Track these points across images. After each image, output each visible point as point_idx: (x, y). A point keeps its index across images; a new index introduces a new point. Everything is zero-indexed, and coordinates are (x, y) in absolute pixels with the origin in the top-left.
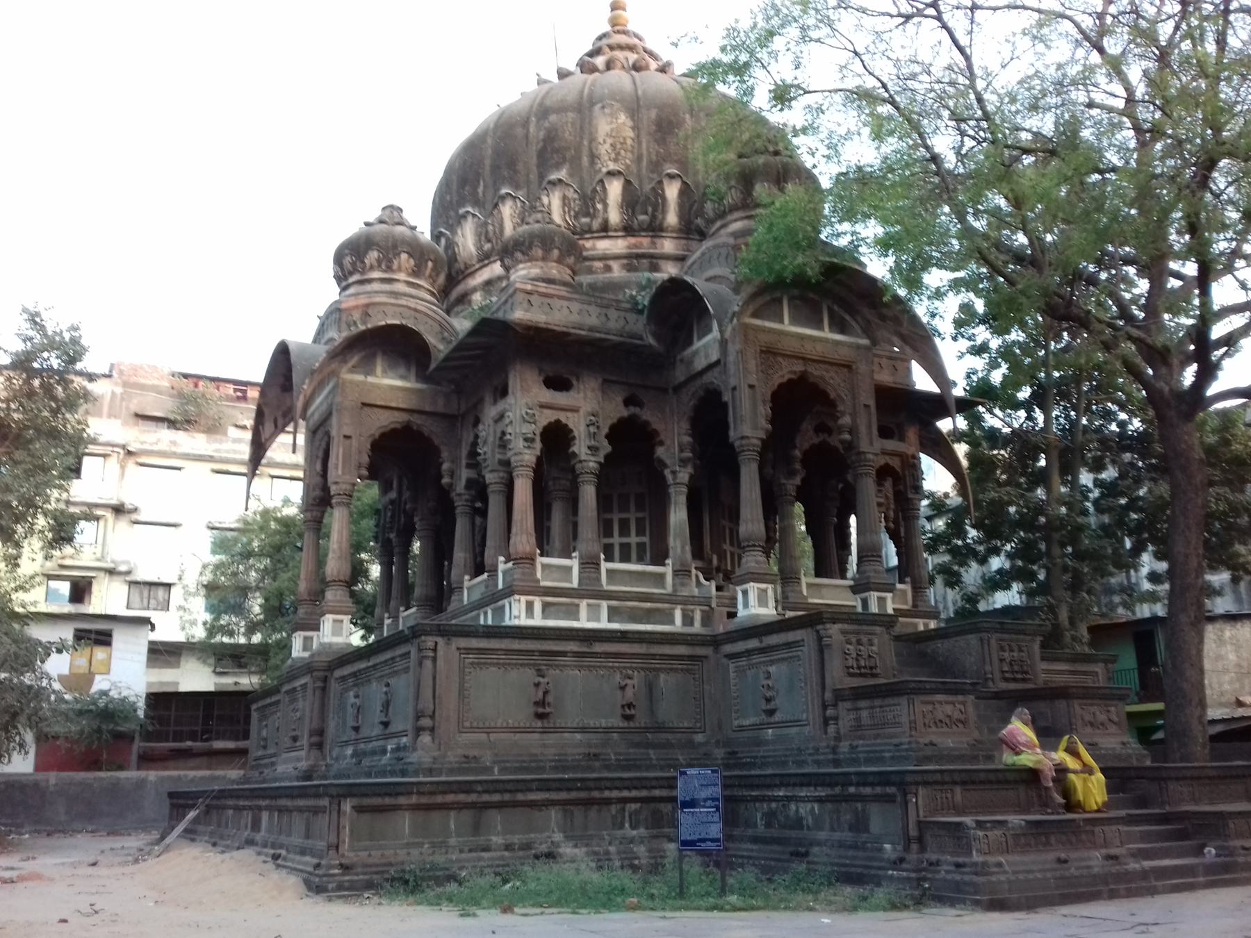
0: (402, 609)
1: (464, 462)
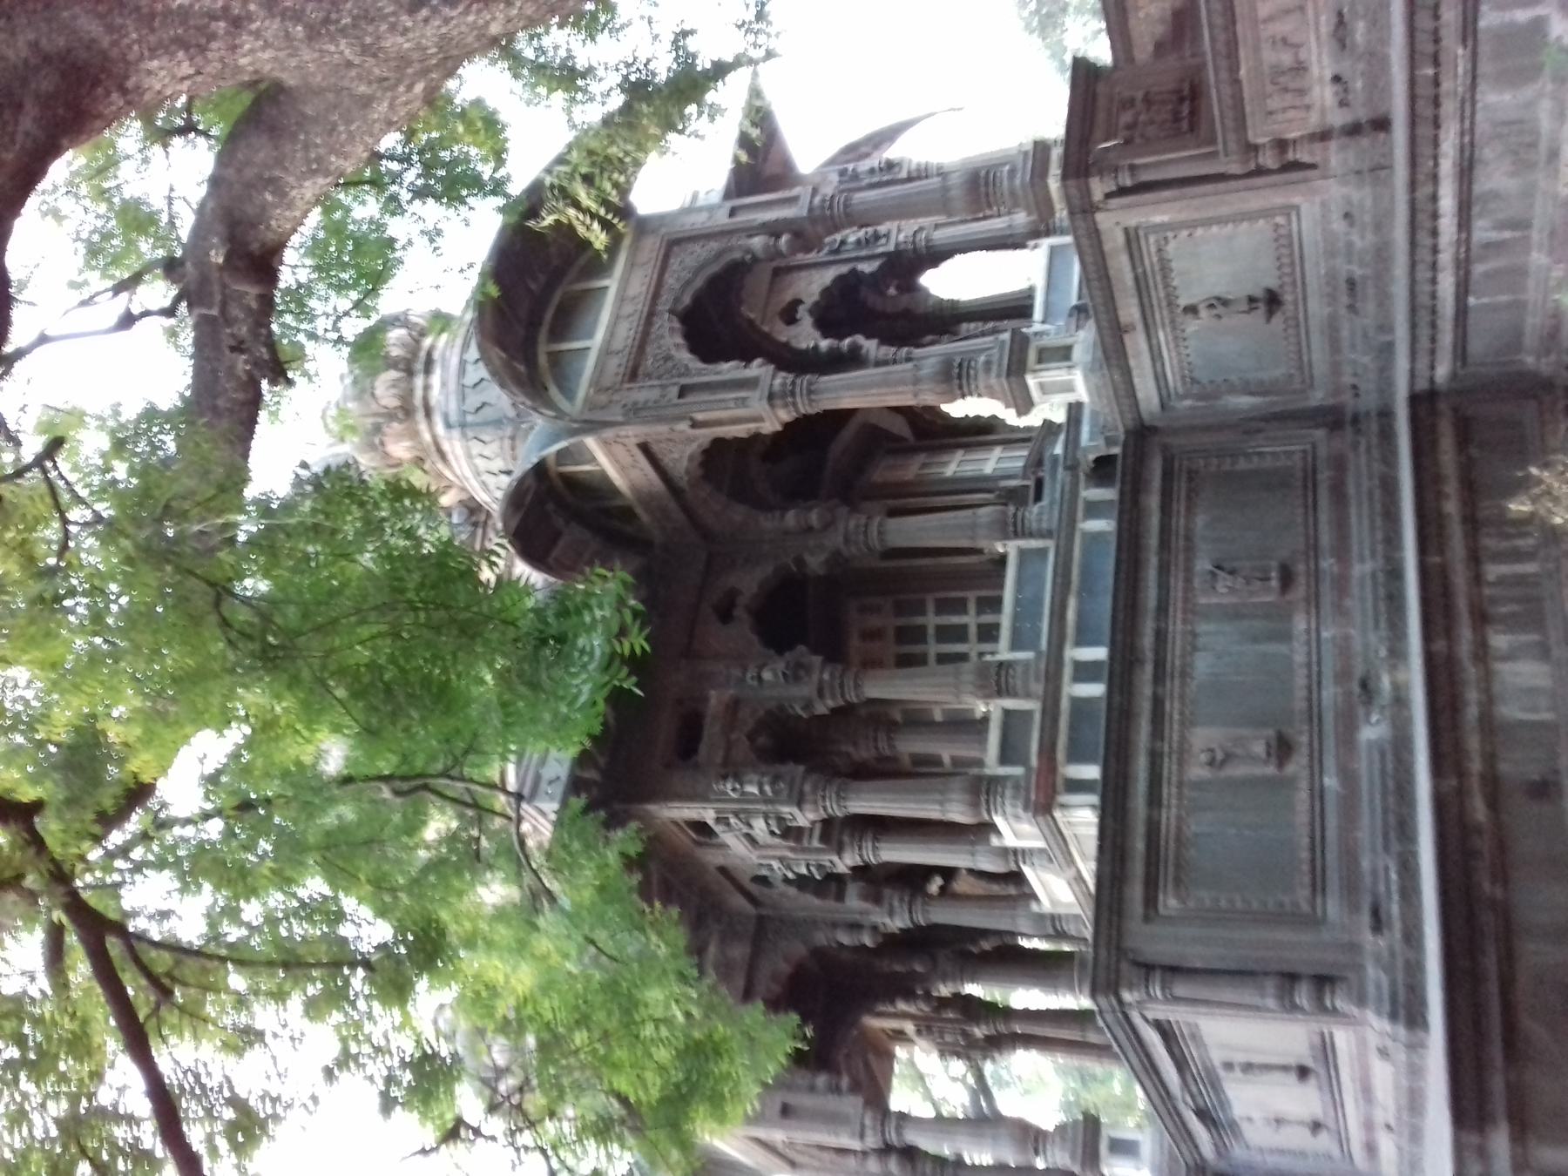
1: (830, 904)
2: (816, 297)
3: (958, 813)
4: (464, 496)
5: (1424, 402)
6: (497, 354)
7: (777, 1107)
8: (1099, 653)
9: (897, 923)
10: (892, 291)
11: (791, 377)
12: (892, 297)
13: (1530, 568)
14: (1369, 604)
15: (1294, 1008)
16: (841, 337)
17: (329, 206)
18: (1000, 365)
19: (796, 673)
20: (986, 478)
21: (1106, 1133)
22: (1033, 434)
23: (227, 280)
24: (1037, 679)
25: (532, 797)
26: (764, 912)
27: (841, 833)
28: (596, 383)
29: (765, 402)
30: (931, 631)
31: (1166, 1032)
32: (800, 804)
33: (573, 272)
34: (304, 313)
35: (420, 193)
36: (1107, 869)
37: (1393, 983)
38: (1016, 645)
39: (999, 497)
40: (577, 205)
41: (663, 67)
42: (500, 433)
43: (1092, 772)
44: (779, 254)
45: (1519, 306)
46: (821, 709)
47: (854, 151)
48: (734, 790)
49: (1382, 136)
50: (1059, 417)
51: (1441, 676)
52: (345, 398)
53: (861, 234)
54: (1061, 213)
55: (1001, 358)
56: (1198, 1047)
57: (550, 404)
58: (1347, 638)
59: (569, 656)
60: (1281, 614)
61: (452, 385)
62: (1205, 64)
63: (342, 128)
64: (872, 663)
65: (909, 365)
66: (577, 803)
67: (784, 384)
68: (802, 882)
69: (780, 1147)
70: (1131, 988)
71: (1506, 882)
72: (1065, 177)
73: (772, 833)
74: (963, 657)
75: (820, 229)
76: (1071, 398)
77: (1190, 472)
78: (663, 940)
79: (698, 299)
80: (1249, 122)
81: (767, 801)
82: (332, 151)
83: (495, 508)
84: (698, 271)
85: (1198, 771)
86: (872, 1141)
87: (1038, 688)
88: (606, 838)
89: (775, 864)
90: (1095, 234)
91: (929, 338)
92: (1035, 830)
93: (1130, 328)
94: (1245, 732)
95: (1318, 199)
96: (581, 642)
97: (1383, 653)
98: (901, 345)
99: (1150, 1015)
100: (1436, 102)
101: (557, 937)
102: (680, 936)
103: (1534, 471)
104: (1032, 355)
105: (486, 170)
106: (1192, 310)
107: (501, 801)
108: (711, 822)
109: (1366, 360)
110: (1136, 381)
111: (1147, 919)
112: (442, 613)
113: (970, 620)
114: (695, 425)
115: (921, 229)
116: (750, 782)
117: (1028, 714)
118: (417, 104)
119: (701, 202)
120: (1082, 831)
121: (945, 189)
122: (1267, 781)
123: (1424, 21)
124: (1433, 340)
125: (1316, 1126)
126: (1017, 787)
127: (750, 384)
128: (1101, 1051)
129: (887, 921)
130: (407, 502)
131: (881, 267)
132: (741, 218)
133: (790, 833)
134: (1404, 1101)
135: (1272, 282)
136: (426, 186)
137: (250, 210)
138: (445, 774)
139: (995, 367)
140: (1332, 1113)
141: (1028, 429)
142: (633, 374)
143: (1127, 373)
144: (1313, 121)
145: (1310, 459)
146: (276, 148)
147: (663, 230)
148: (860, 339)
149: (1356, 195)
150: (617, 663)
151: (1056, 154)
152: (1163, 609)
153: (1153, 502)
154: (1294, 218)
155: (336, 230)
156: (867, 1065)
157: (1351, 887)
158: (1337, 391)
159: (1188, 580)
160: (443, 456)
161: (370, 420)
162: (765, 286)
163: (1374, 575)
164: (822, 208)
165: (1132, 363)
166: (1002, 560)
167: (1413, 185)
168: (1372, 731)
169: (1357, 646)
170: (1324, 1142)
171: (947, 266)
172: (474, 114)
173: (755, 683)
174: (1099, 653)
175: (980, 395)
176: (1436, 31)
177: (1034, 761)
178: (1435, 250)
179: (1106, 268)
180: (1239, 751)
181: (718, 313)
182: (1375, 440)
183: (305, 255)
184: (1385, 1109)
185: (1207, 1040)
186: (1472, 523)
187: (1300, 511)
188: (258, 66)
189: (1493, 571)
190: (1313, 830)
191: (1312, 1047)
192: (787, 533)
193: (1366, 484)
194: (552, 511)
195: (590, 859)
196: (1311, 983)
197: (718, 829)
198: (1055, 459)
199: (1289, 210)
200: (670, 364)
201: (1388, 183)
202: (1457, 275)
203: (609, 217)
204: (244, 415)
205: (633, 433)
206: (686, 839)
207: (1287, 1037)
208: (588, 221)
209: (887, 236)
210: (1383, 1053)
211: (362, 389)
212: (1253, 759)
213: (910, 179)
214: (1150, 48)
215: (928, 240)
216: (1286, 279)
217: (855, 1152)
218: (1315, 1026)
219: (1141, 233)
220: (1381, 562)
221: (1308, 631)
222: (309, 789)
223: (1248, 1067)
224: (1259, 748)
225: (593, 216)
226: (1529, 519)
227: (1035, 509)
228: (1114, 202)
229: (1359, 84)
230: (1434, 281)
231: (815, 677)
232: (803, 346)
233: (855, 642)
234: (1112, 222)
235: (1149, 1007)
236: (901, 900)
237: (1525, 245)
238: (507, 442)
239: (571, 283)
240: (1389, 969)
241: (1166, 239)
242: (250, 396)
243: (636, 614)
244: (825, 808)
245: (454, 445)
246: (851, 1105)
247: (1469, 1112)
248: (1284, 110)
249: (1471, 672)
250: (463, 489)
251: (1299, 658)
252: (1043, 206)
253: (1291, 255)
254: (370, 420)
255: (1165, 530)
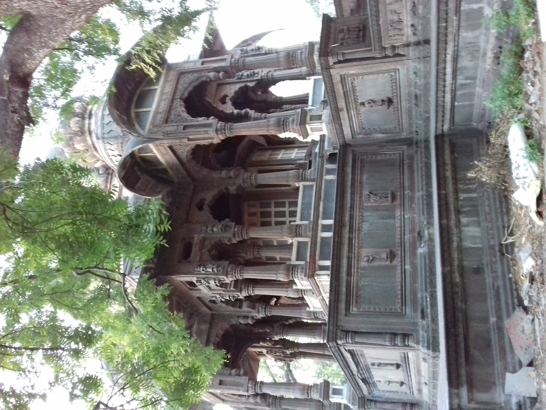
0: (308, 309)
1: (238, 309)
2: (233, 94)
3: (282, 278)
4: (103, 164)
5: (439, 138)
6: (116, 112)
7: (218, 382)
8: (331, 222)
9: (260, 316)
10: (260, 93)
11: (224, 123)
12: (260, 95)
13: (474, 195)
14: (421, 206)
15: (395, 345)
16: (242, 110)
17: (52, 57)
18: (297, 121)
19: (225, 229)
20: (292, 160)
21: (332, 387)
22: (308, 145)
23: (10, 86)
24: (309, 231)
25: (130, 273)
26: (214, 312)
27: (241, 285)
28: (153, 124)
29: (214, 132)
30: (273, 213)
31: (352, 353)
32: (227, 275)
33: (144, 83)
34: (42, 96)
35: (87, 53)
36: (333, 298)
37: (428, 336)
38: (302, 219)
39: (296, 166)
40: (144, 62)
41: (176, 12)
42: (117, 141)
43: (328, 263)
44: (220, 79)
45: (472, 106)
46: (234, 241)
47: (246, 43)
48: (203, 270)
49: (427, 46)
50: (317, 138)
51: (445, 232)
52: (59, 127)
53: (249, 72)
54: (318, 68)
55: (297, 119)
56: (363, 358)
57: (136, 131)
58: (413, 218)
59: (140, 232)
60: (392, 210)
61: (99, 123)
62: (368, 18)
63: (54, 31)
64: (253, 225)
65: (265, 120)
66: (146, 276)
67: (221, 126)
68: (227, 302)
69: (219, 395)
70: (341, 340)
71: (466, 304)
72: (320, 56)
73: (217, 285)
74: (284, 223)
75: (234, 70)
76: (322, 133)
77: (362, 160)
78: (177, 325)
79: (190, 94)
80: (383, 39)
81: (215, 274)
82: (51, 39)
83: (116, 168)
84: (190, 83)
85: (363, 264)
86: (251, 392)
87: (310, 234)
88: (157, 289)
89: (218, 296)
90: (330, 76)
91: (272, 110)
92: (308, 283)
93: (342, 110)
94: (378, 250)
95: (405, 67)
96: (145, 227)
97: (425, 223)
98: (263, 112)
99: (347, 348)
100: (446, 36)
101: (138, 325)
102: (184, 324)
103: (476, 162)
104: (308, 118)
105: (112, 47)
106: (363, 104)
107: (118, 277)
108: (195, 282)
109: (421, 122)
110: (344, 128)
111: (346, 315)
112: (91, 216)
113: (286, 209)
114: (189, 140)
115: (270, 71)
116: (209, 268)
117: (307, 242)
118: (83, 22)
119: (191, 59)
120: (324, 283)
121: (278, 58)
122: (386, 267)
123: (443, 7)
124: (443, 117)
125: (402, 384)
126: (302, 269)
127: (209, 125)
128: (329, 357)
129: (257, 315)
130: (79, 173)
131: (255, 85)
132: (206, 65)
133: (223, 285)
134: (431, 375)
135: (390, 95)
136: (89, 50)
137: (19, 60)
138: (96, 267)
139: (295, 122)
140: (407, 379)
141: (307, 143)
142: (166, 121)
143: (341, 125)
144: (404, 40)
145: (402, 155)
146: (29, 38)
147: (178, 69)
148: (248, 110)
149: (418, 66)
150: (159, 235)
151: (317, 47)
152: (352, 207)
153: (349, 170)
154: (397, 73)
155: (55, 65)
156: (250, 365)
157: (414, 303)
158: (411, 133)
159: (361, 197)
160: (96, 149)
161: (68, 136)
162: (214, 90)
163: (422, 196)
164: (235, 63)
165: (342, 121)
166: (298, 189)
167: (438, 64)
168: (422, 250)
169: (417, 221)
170: (404, 388)
171: (279, 84)
172: (105, 27)
173: (211, 232)
174: (331, 222)
175: (290, 132)
176: (447, 11)
177: (308, 260)
178: (444, 86)
179: (334, 88)
180: (377, 257)
181: (197, 100)
182: (423, 150)
183: (43, 75)
184: (425, 378)
185: (366, 356)
186: (455, 180)
187: (398, 174)
188: (21, 7)
189: (462, 196)
190: (402, 283)
191: (401, 357)
192: (222, 179)
193: (420, 165)
194: (136, 171)
195: (150, 296)
196: (401, 337)
197: (197, 284)
198: (316, 153)
199: (396, 70)
200: (180, 118)
201: (429, 62)
202: (451, 95)
203: (156, 66)
204: (17, 136)
205: (167, 143)
206: (185, 288)
207: (393, 354)
208: (148, 67)
209: (258, 73)
210: (425, 360)
211: (65, 125)
212: (381, 259)
213: (266, 54)
214: (349, 11)
215: (272, 75)
216: (395, 94)
217: (245, 396)
218: (403, 351)
219: (346, 77)
220: (425, 192)
221: (401, 216)
222: (45, 274)
223: (379, 365)
224: (384, 256)
225: (151, 66)
226: (474, 179)
227: (309, 171)
228: (337, 66)
229: (420, 28)
230: (444, 97)
231: (232, 230)
232: (228, 112)
233: (246, 217)
234: (336, 72)
235: (346, 345)
236: (262, 308)
237: (474, 85)
238: (120, 145)
239: (145, 86)
240: (427, 331)
241: (354, 79)
242: (19, 129)
243: (166, 216)
244: (235, 277)
245: (99, 145)
246: (244, 380)
247: (454, 381)
248: (394, 36)
249: (455, 230)
250: (103, 161)
251: (398, 225)
252: (312, 66)
253: (396, 86)
254: (68, 136)
255: (353, 180)
